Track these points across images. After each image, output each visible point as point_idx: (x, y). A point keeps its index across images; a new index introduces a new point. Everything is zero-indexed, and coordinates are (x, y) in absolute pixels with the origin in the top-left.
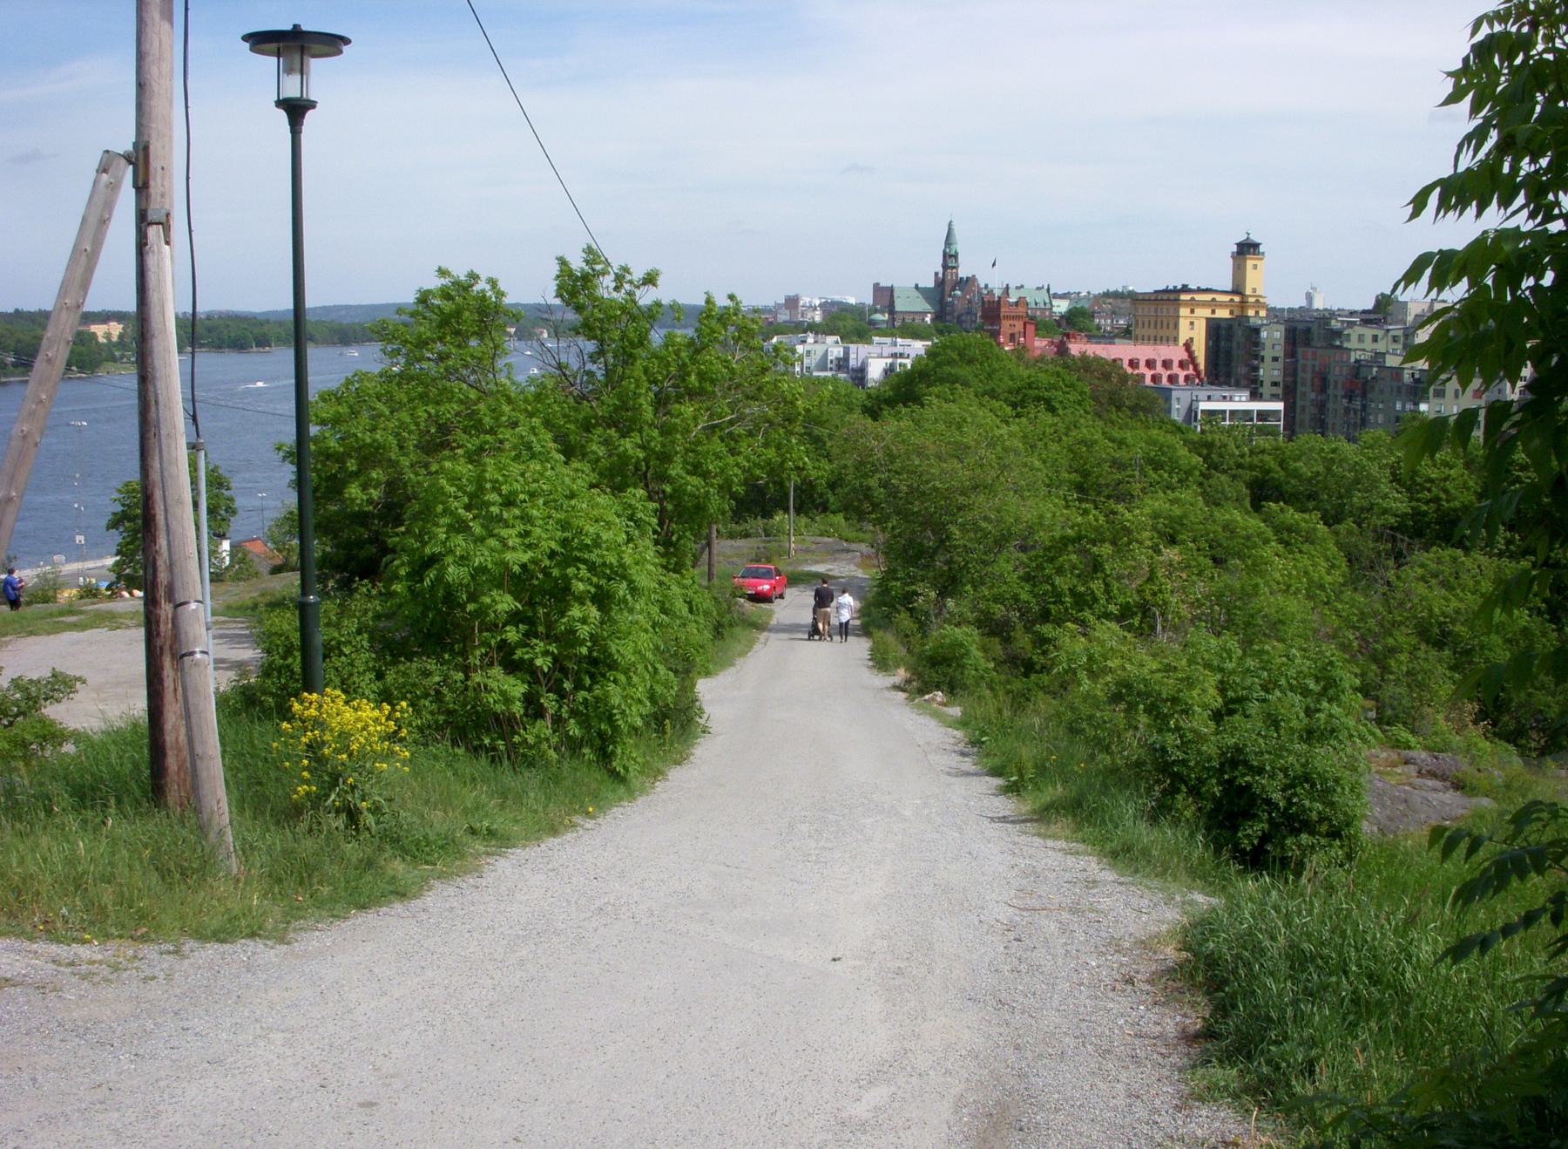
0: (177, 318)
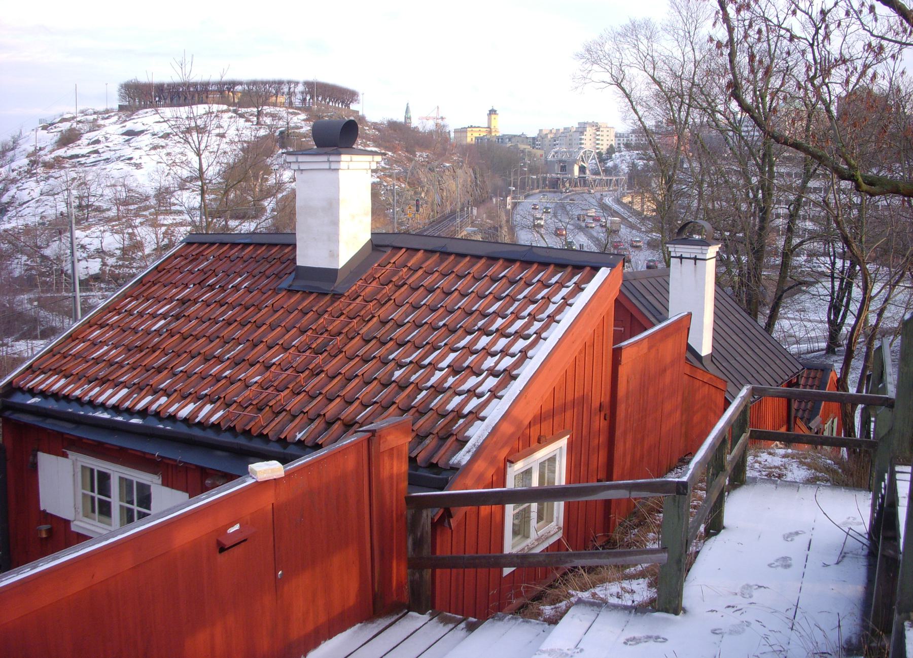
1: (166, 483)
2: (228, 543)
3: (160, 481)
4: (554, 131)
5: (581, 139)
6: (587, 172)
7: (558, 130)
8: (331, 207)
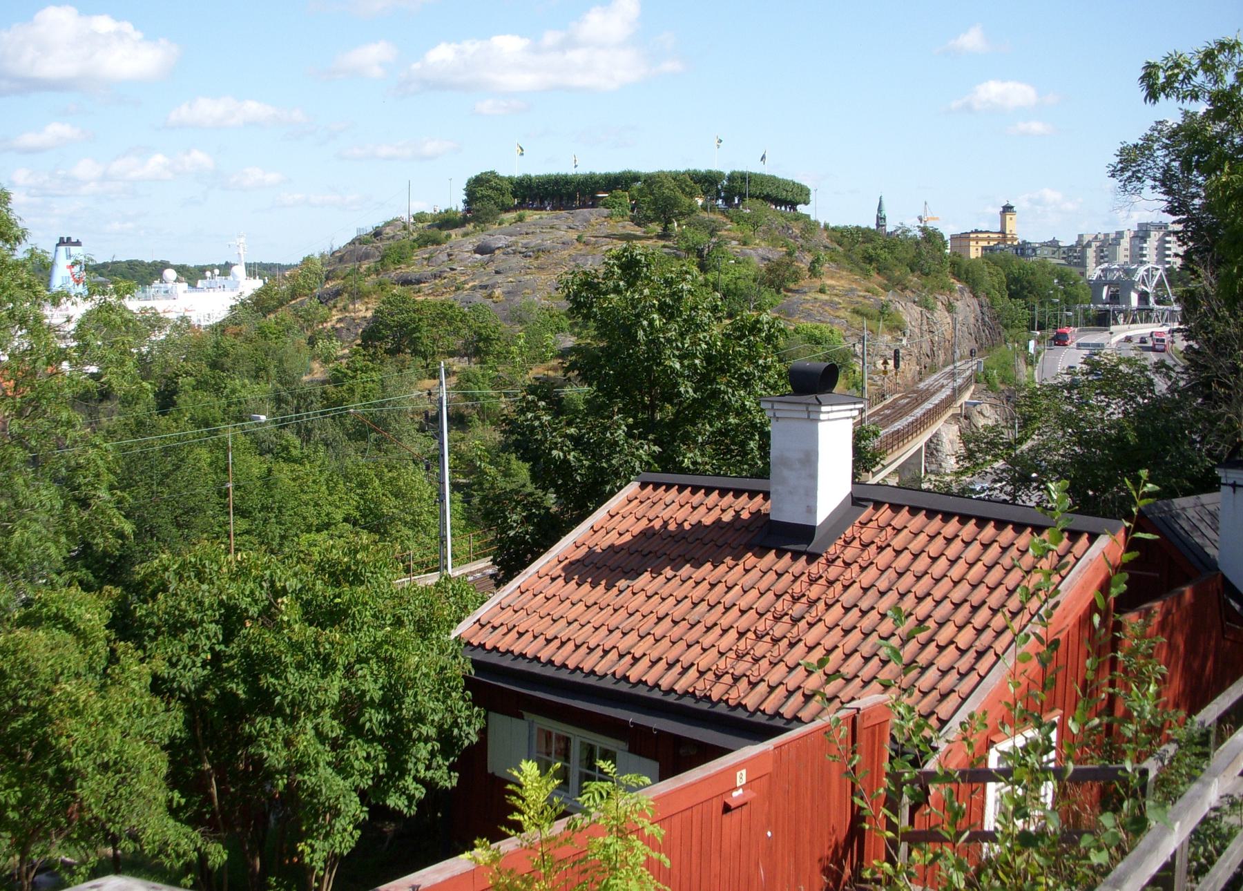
0: (662, 777)
1: (632, 750)
2: (733, 805)
3: (627, 748)
4: (1101, 237)
5: (1142, 249)
6: (1152, 300)
7: (1107, 235)
8: (809, 461)
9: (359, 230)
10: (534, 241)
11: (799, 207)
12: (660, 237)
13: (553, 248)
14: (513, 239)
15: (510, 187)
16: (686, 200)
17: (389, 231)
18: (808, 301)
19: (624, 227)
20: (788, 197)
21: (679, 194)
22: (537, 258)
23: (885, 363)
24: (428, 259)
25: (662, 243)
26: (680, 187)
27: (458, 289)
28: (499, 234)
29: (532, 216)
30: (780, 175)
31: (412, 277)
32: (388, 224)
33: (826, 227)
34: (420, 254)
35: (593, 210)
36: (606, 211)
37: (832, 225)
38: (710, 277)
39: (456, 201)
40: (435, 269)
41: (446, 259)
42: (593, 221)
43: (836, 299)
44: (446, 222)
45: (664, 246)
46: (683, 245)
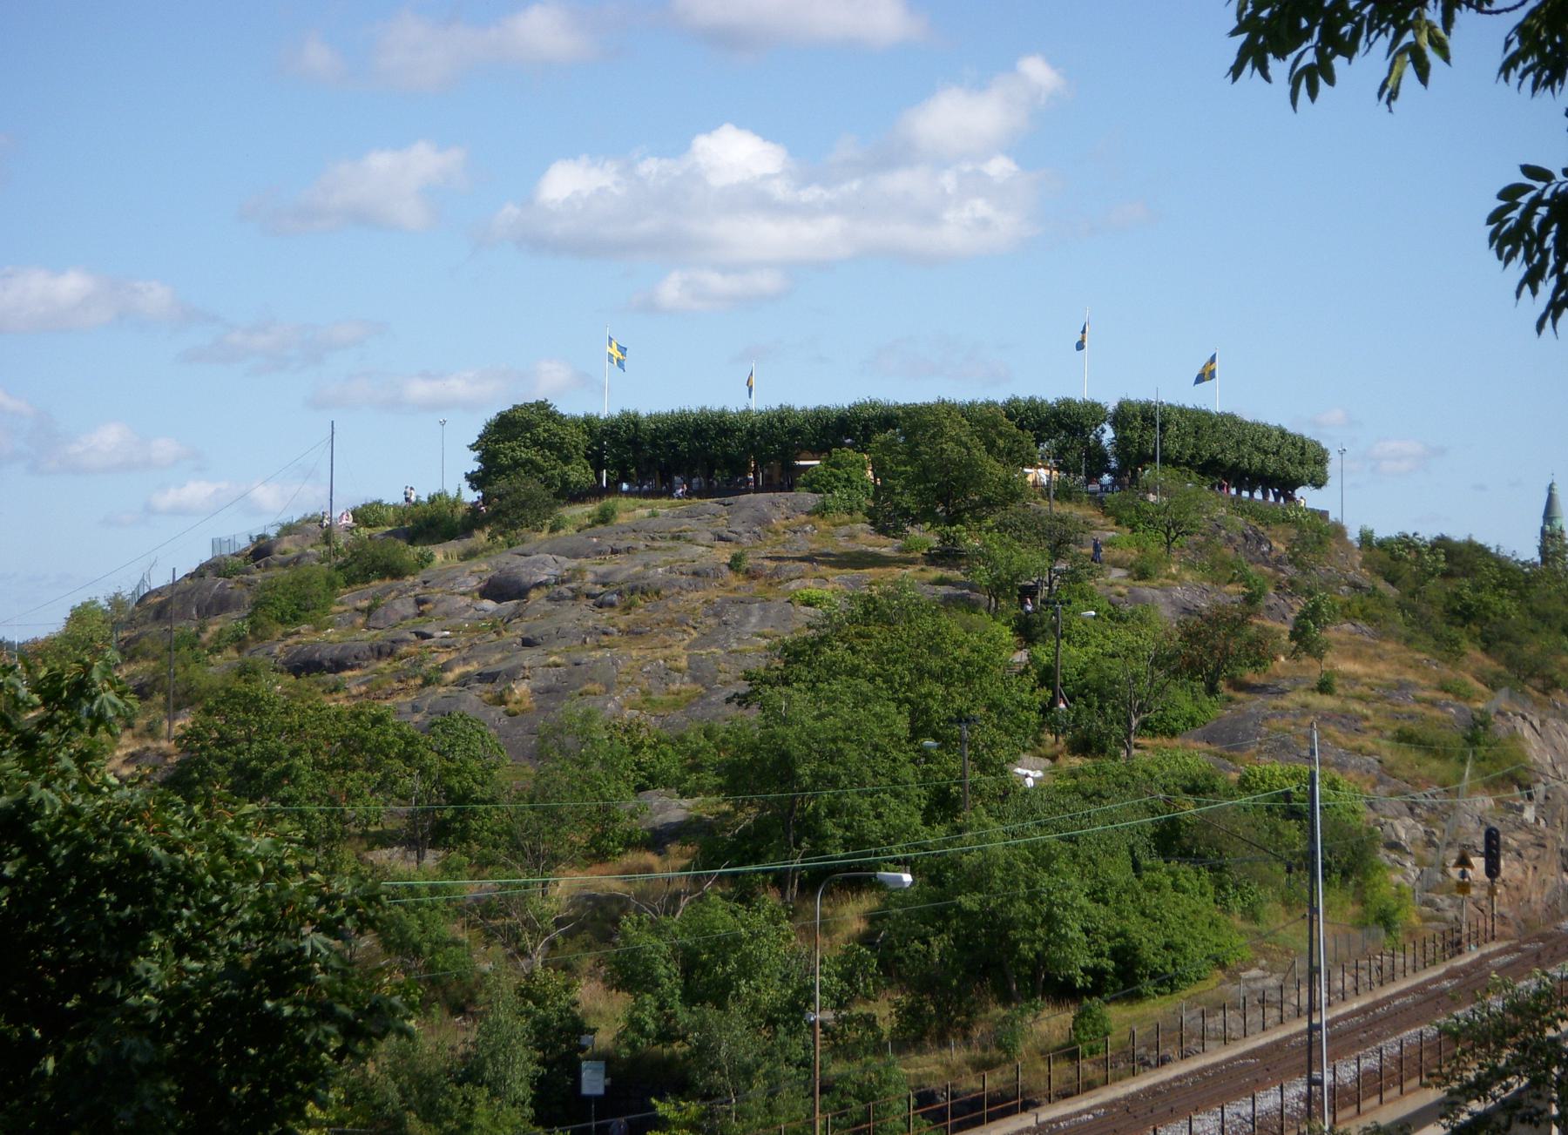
9: (216, 543)
10: (625, 568)
11: (1300, 492)
12: (933, 559)
13: (670, 584)
14: (573, 563)
15: (582, 439)
16: (995, 469)
17: (289, 546)
18: (1283, 712)
19: (852, 537)
20: (1267, 466)
21: (979, 453)
22: (627, 609)
23: (1463, 862)
24: (369, 611)
25: (935, 573)
26: (984, 436)
27: (427, 682)
28: (538, 557)
29: (632, 510)
30: (1248, 414)
31: (325, 654)
32: (288, 530)
33: (1366, 539)
34: (353, 598)
35: (780, 497)
36: (809, 499)
37: (1381, 533)
38: (1042, 653)
39: (445, 471)
40: (378, 636)
41: (410, 610)
42: (777, 522)
43: (1357, 707)
44: (429, 524)
45: (942, 582)
46: (983, 575)
